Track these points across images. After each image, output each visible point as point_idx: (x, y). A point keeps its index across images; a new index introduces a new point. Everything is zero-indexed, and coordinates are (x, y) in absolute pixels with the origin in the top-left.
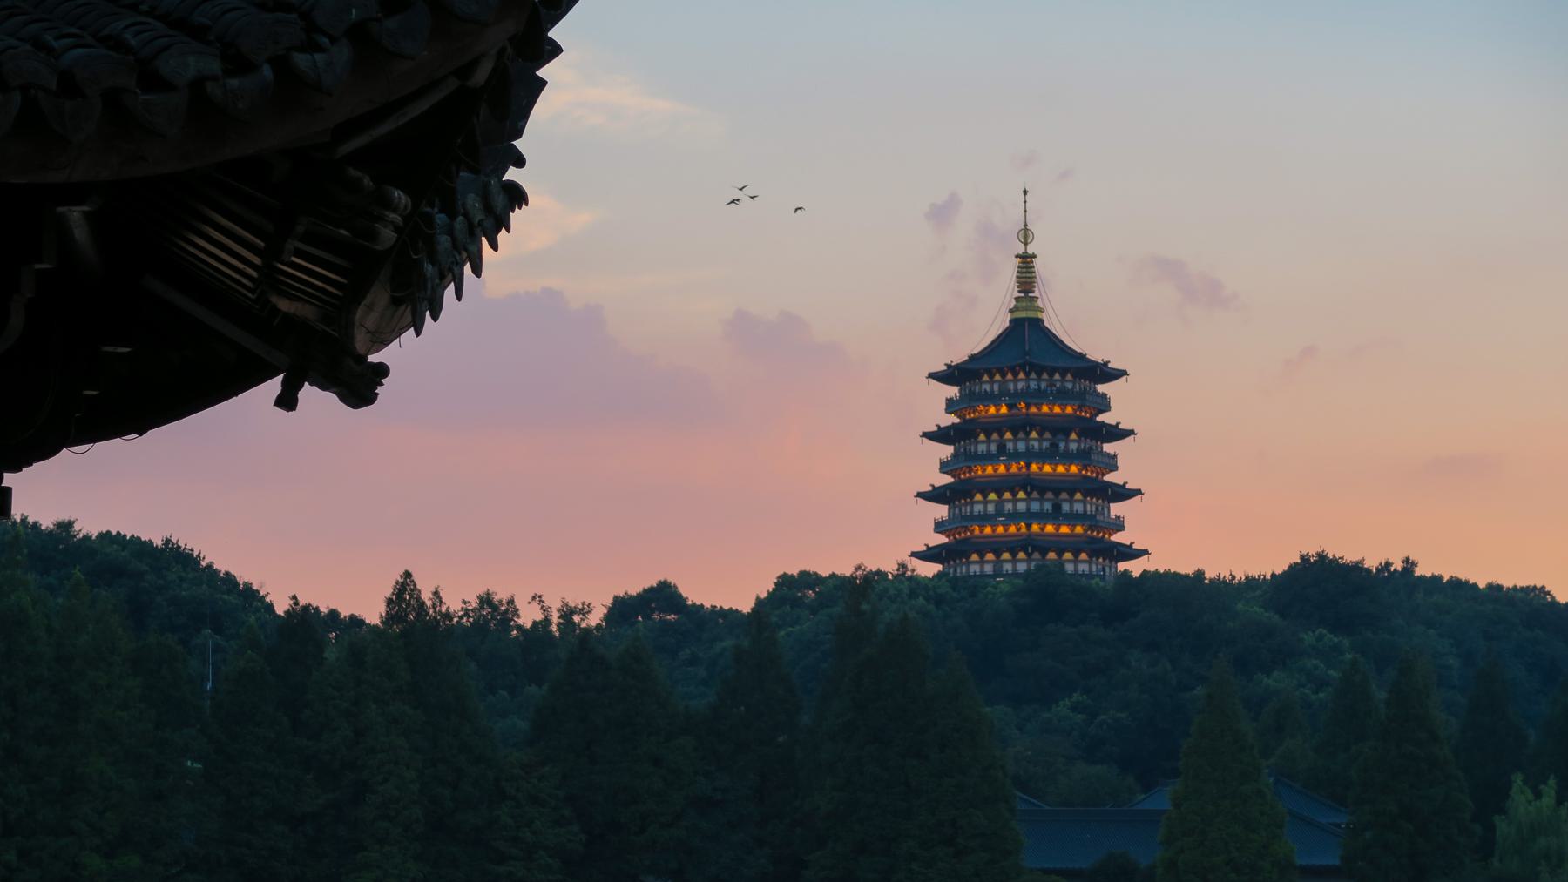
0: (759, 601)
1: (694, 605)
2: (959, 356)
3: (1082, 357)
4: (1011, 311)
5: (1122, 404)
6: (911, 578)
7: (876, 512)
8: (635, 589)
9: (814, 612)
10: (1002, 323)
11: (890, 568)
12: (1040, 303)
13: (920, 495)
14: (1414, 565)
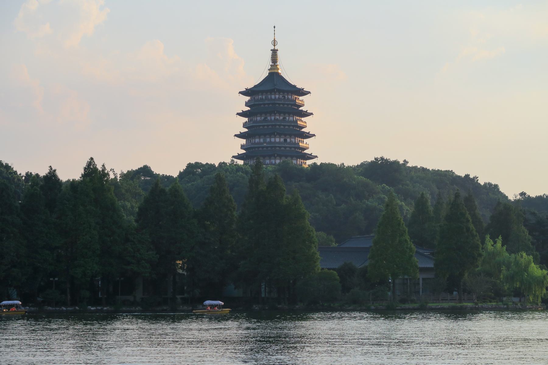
0: (180, 173)
1: (156, 174)
2: (250, 86)
3: (294, 87)
4: (269, 70)
5: (307, 103)
6: (235, 165)
7: (221, 143)
8: (135, 168)
9: (201, 177)
10: (266, 74)
11: (228, 161)
12: (278, 67)
13: (236, 135)
14: (407, 162)
